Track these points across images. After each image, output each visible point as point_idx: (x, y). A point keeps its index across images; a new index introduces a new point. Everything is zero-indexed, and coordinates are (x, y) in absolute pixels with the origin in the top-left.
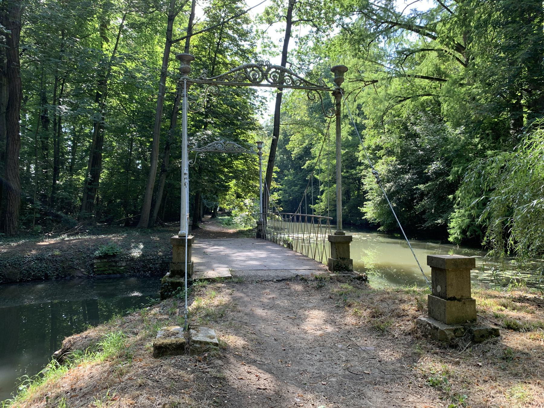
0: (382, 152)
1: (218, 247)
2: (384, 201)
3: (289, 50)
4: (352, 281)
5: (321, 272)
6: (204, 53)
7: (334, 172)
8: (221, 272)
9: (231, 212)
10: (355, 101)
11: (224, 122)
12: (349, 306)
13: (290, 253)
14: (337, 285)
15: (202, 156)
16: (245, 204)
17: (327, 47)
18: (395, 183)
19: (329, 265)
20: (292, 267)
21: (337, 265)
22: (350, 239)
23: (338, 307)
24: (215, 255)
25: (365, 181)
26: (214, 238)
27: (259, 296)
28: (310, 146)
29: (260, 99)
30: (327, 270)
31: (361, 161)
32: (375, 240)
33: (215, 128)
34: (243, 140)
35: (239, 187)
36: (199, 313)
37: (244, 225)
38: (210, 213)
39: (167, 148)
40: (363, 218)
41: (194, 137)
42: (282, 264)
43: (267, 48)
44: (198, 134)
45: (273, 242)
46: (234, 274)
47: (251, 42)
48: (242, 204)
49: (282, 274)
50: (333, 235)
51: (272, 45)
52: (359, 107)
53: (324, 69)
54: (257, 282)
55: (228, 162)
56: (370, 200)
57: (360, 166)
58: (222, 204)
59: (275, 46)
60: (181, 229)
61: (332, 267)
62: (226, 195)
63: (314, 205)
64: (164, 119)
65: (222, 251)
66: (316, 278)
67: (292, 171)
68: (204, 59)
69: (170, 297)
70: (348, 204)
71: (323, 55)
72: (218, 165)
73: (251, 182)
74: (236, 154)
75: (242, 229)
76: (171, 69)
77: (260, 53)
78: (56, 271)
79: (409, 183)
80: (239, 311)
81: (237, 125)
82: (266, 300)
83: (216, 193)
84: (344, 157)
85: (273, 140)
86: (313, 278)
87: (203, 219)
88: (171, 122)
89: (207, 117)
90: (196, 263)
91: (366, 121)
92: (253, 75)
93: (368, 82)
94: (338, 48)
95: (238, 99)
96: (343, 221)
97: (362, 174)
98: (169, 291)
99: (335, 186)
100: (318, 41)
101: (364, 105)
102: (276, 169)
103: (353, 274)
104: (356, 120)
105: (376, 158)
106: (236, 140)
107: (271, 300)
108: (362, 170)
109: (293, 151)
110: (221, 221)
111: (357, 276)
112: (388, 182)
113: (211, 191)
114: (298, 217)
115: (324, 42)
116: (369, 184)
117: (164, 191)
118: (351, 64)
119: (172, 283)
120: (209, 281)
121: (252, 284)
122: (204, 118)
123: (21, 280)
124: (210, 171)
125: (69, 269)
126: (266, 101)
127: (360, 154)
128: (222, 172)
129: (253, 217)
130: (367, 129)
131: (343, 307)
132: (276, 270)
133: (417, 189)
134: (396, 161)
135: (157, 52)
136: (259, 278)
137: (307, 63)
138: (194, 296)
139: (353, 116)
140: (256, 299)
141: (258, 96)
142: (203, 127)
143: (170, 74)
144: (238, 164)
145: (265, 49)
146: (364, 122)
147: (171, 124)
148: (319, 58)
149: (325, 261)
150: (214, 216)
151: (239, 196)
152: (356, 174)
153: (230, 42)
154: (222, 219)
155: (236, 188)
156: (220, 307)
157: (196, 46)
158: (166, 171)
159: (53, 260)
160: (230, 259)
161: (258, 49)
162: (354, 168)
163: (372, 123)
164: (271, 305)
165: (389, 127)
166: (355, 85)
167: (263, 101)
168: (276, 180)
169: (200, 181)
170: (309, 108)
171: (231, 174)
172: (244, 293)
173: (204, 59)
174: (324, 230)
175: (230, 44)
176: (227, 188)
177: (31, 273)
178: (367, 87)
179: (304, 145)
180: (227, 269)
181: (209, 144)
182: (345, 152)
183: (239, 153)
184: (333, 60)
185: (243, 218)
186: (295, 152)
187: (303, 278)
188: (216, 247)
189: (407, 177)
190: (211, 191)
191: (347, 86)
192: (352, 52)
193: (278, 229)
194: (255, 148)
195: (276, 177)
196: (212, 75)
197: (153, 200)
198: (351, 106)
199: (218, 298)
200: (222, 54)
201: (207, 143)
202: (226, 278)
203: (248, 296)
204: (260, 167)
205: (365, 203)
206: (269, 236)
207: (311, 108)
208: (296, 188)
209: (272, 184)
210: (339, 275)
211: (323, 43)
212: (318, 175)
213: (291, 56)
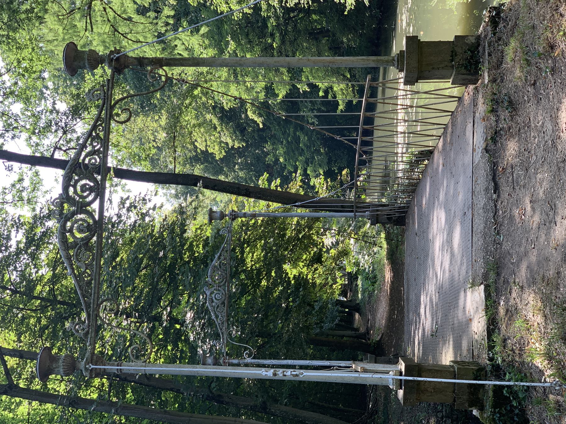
1: (422, 306)
3: (27, 151)
4: (499, 39)
5: (481, 100)
6: (32, 321)
8: (475, 306)
9: (349, 274)
10: (130, 19)
11: (169, 285)
12: (552, 47)
13: (438, 158)
14: (507, 70)
15: (235, 332)
16: (335, 245)
17: (23, 75)
19: (465, 83)
20: (468, 159)
21: (466, 68)
22: (412, 40)
23: (553, 70)
24: (440, 315)
26: (401, 312)
27: (527, 231)
28: (217, 110)
29: (124, 211)
30: (476, 88)
33: (179, 303)
34: (204, 247)
35: (299, 259)
36: (558, 354)
37: (376, 249)
38: (351, 316)
39: (219, 399)
41: (197, 346)
42: (461, 180)
43: (24, 194)
44: (192, 338)
45: (414, 191)
46: (479, 280)
47: (13, 226)
48: (333, 252)
49: (483, 181)
50: (402, 75)
51: (18, 186)
52: (142, 11)
53: (65, 80)
54: (498, 234)
55: (247, 278)
57: (260, 9)
58: (333, 293)
59: (21, 180)
60: (384, 383)
61: (469, 77)
62: (314, 284)
64: (160, 404)
65: (431, 300)
66: (493, 111)
67: (268, 147)
68: (44, 322)
69: (523, 411)
70: (338, 34)
71: (39, 84)
72: (254, 298)
73: (288, 233)
74: (233, 263)
75: (385, 253)
76: (63, 386)
77: (34, 210)
80: (558, 273)
81: (174, 259)
82: (537, 218)
83: (309, 305)
84: (243, 42)
85: (206, 187)
87: (362, 330)
88: (167, 390)
89: (158, 318)
90: (455, 356)
92: (80, 231)
94: (26, 53)
95: (123, 255)
96: (376, 55)
98: (512, 411)
100: (12, 93)
102: (262, 182)
103: (486, 36)
104: (168, 17)
106: (205, 260)
107: (536, 206)
108: (269, 5)
109: (227, 144)
110: (366, 294)
111: (489, 28)
113: (307, 314)
114: (364, 143)
115: (13, 81)
117: (303, 408)
118: (57, 27)
119: (494, 406)
120: (493, 330)
122: (161, 325)
124: (266, 316)
126: (128, 198)
128: (269, 290)
129: (360, 227)
131: (555, 60)
132: (473, 192)
135: (29, 414)
136: (489, 229)
137: (55, 115)
138: (523, 363)
139: (160, 24)
140: (532, 236)
141: (119, 216)
142: (178, 326)
143: (72, 389)
145: (26, 198)
147: (172, 390)
148: (44, 90)
149: (456, 91)
150: (355, 307)
151: (317, 259)
152: (277, 17)
153: (12, 268)
154: (364, 291)
155: (301, 264)
156: (547, 311)
157: (19, 335)
158: (264, 402)
160: (446, 285)
161: (26, 213)
162: (265, 21)
164: (547, 208)
166: (99, 19)
167: (127, 205)
168: (286, 180)
169: (285, 336)
170: (142, 111)
171: (273, 274)
172: (520, 260)
173: (44, 322)
174: (389, 93)
175: (16, 267)
176: (301, 281)
179: (215, 121)
180: (469, 293)
181: (213, 317)
182: (232, 42)
183: (231, 258)
184: (49, 63)
185: (361, 248)
186: (229, 141)
187: (492, 138)
188: (422, 311)
190: (307, 314)
191: (99, 34)
192: (34, 25)
193: (386, 175)
194: (220, 224)
195: (278, 181)
196: (75, 306)
197: (308, 366)
199: (530, 315)
200: (35, 286)
201: (210, 319)
202: (488, 296)
203: (526, 254)
204: (260, 215)
206: (402, 200)
207: (143, 107)
208: (304, 138)
209: (293, 191)
210: (486, 64)
211: (16, 83)
212: (277, 95)
213: (41, 148)
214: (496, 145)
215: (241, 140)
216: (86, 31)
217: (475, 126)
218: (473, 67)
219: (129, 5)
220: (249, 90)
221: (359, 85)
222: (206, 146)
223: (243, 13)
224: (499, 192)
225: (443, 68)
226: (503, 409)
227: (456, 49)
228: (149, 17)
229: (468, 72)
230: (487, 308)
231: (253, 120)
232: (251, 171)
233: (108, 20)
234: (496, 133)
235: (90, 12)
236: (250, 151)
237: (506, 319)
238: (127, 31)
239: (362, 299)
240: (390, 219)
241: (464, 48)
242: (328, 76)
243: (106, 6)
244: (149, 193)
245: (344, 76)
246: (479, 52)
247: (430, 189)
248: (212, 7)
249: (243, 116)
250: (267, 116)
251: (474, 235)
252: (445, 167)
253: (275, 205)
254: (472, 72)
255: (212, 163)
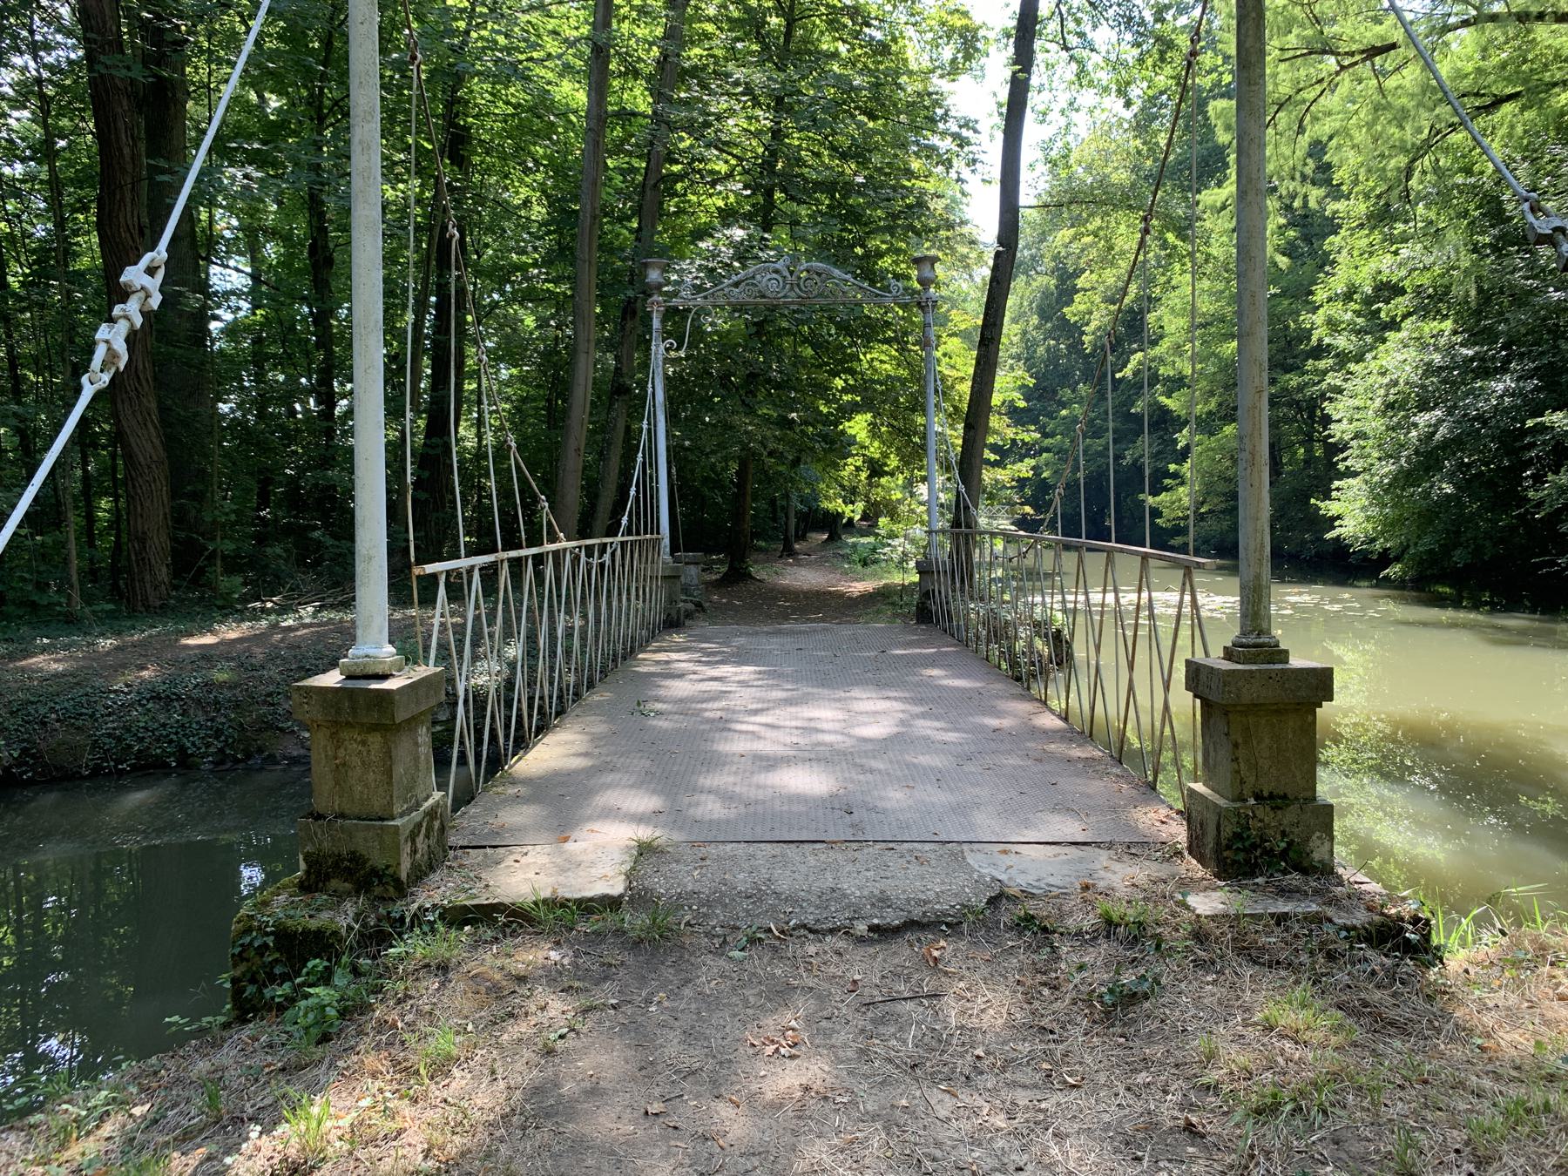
0: (1401, 304)
2: (1405, 478)
7: (1229, 378)
18: (1450, 412)
20: (986, 825)
21: (1237, 836)
25: (1337, 409)
31: (1320, 340)
32: (1371, 613)
40: (1329, 535)
52: (1317, 148)
56: (1355, 474)
57: (1318, 358)
61: (1210, 841)
63: (1155, 493)
66: (1110, 925)
78: (217, 738)
79: (1506, 411)
86: (1089, 922)
91: (1340, 206)
93: (1352, 54)
97: (1324, 385)
99: (1229, 429)
101: (1334, 142)
103: (1334, 902)
104: (1306, 196)
105: (1380, 329)
108: (1325, 372)
111: (1360, 918)
112: (1423, 406)
116: (1351, 421)
121: (720, 951)
123: (96, 772)
125: (260, 729)
126: (976, 131)
127: (1319, 318)
130: (1343, 232)
133: (1541, 429)
134: (1455, 332)
144: (880, 360)
146: (1332, 207)
159: (209, 699)
162: (1297, 369)
163: (1361, 208)
165: (1432, 215)
167: (965, 133)
177: (130, 747)
178: (1345, 75)
186: (1093, 326)
187: (1029, 919)
189: (1501, 386)
198: (1286, 151)
205: (1336, 484)
212: (1169, 397)
214: (1011, 929)
215: (1095, 345)
216: (1281, 49)
217: (1073, 849)
218: (1241, 857)
219: (1326, 127)
220: (1177, 349)
221: (1187, 527)
222: (1086, 290)
223: (1312, 329)
224: (871, 942)
225: (1238, 772)
226: (277, 955)
227: (1294, 808)
228: (1305, 164)
229: (1224, 842)
230: (554, 904)
231: (1128, 361)
232: (1046, 366)
233: (1300, 90)
234: (1045, 930)
235: (1316, 53)
236: (1077, 362)
237: (498, 977)
238: (1280, 128)
239: (847, 544)
240: (926, 595)
241: (1296, 831)
242: (1203, 477)
243: (1325, 84)
244: (987, 168)
245: (1202, 503)
246: (1285, 872)
247: (957, 689)
248: (1322, 275)
249: (1135, 346)
250: (1135, 384)
251: (777, 849)
252: (993, 736)
253: (965, 388)
254: (1225, 854)
255: (1057, 303)
